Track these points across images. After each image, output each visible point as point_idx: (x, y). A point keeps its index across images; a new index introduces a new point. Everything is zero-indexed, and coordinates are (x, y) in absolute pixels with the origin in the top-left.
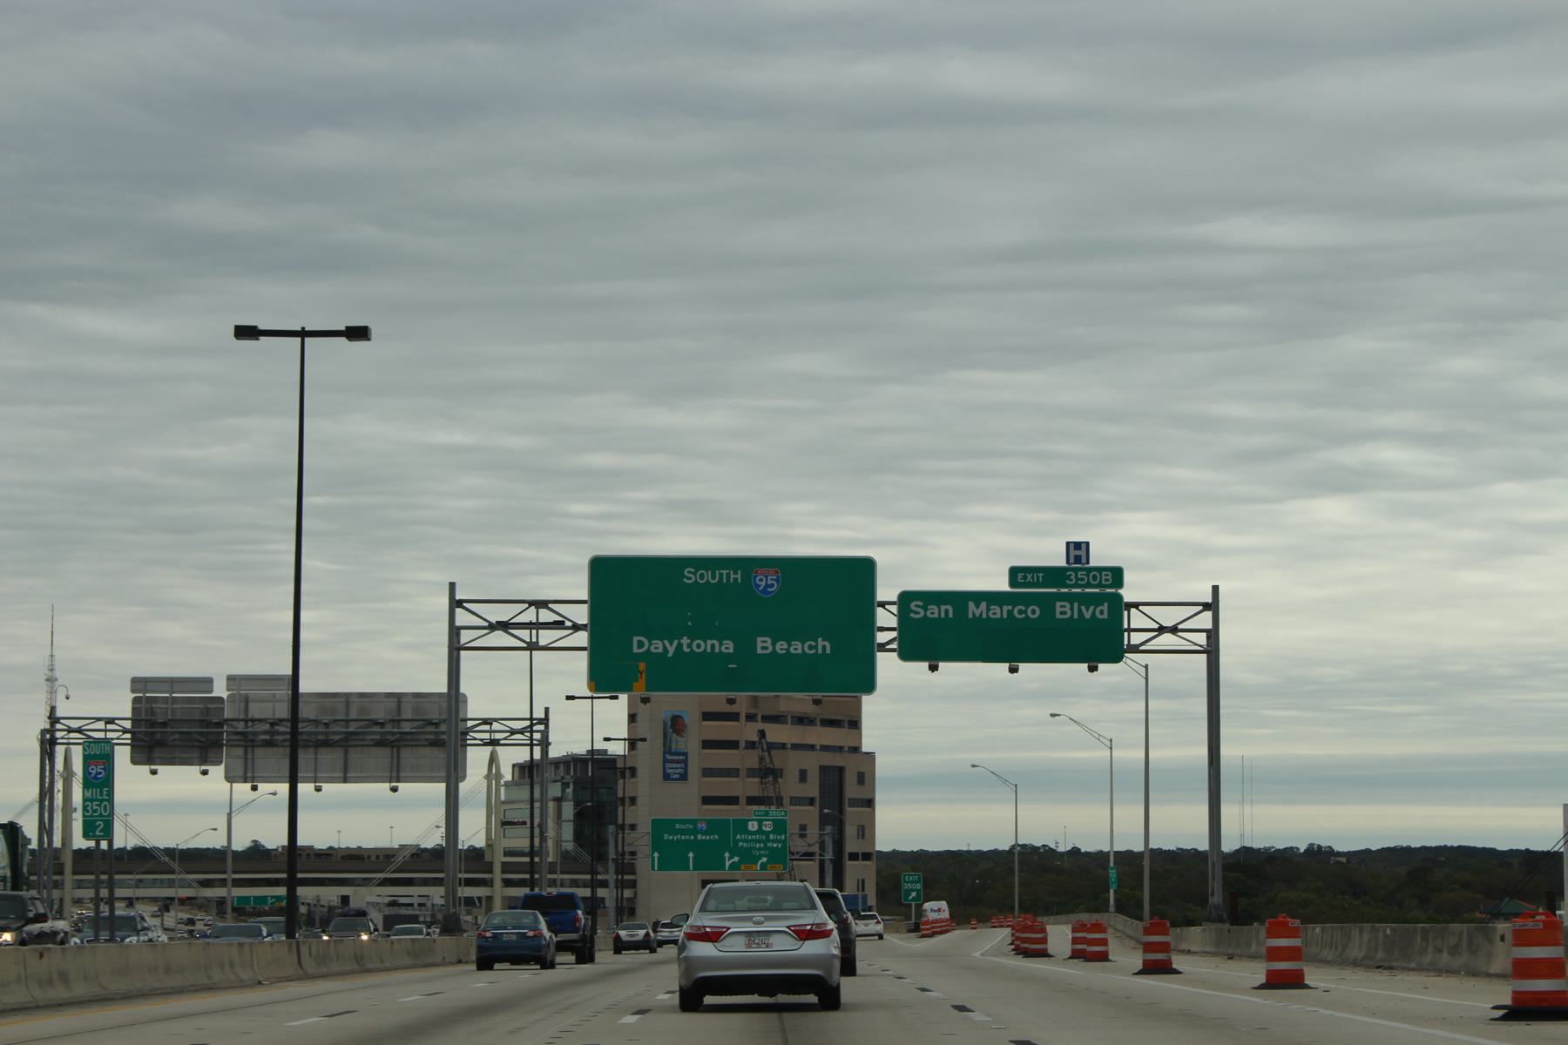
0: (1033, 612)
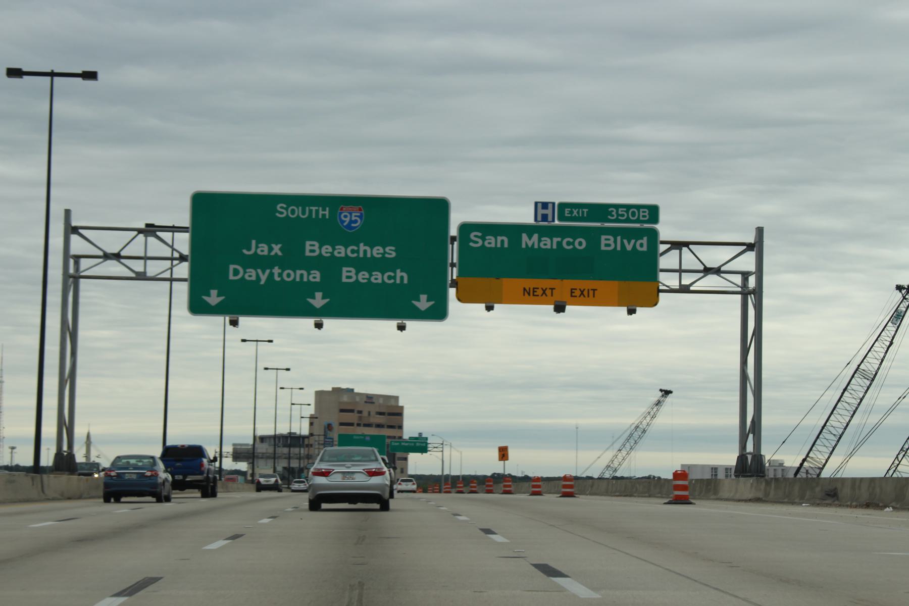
0: (580, 244)
